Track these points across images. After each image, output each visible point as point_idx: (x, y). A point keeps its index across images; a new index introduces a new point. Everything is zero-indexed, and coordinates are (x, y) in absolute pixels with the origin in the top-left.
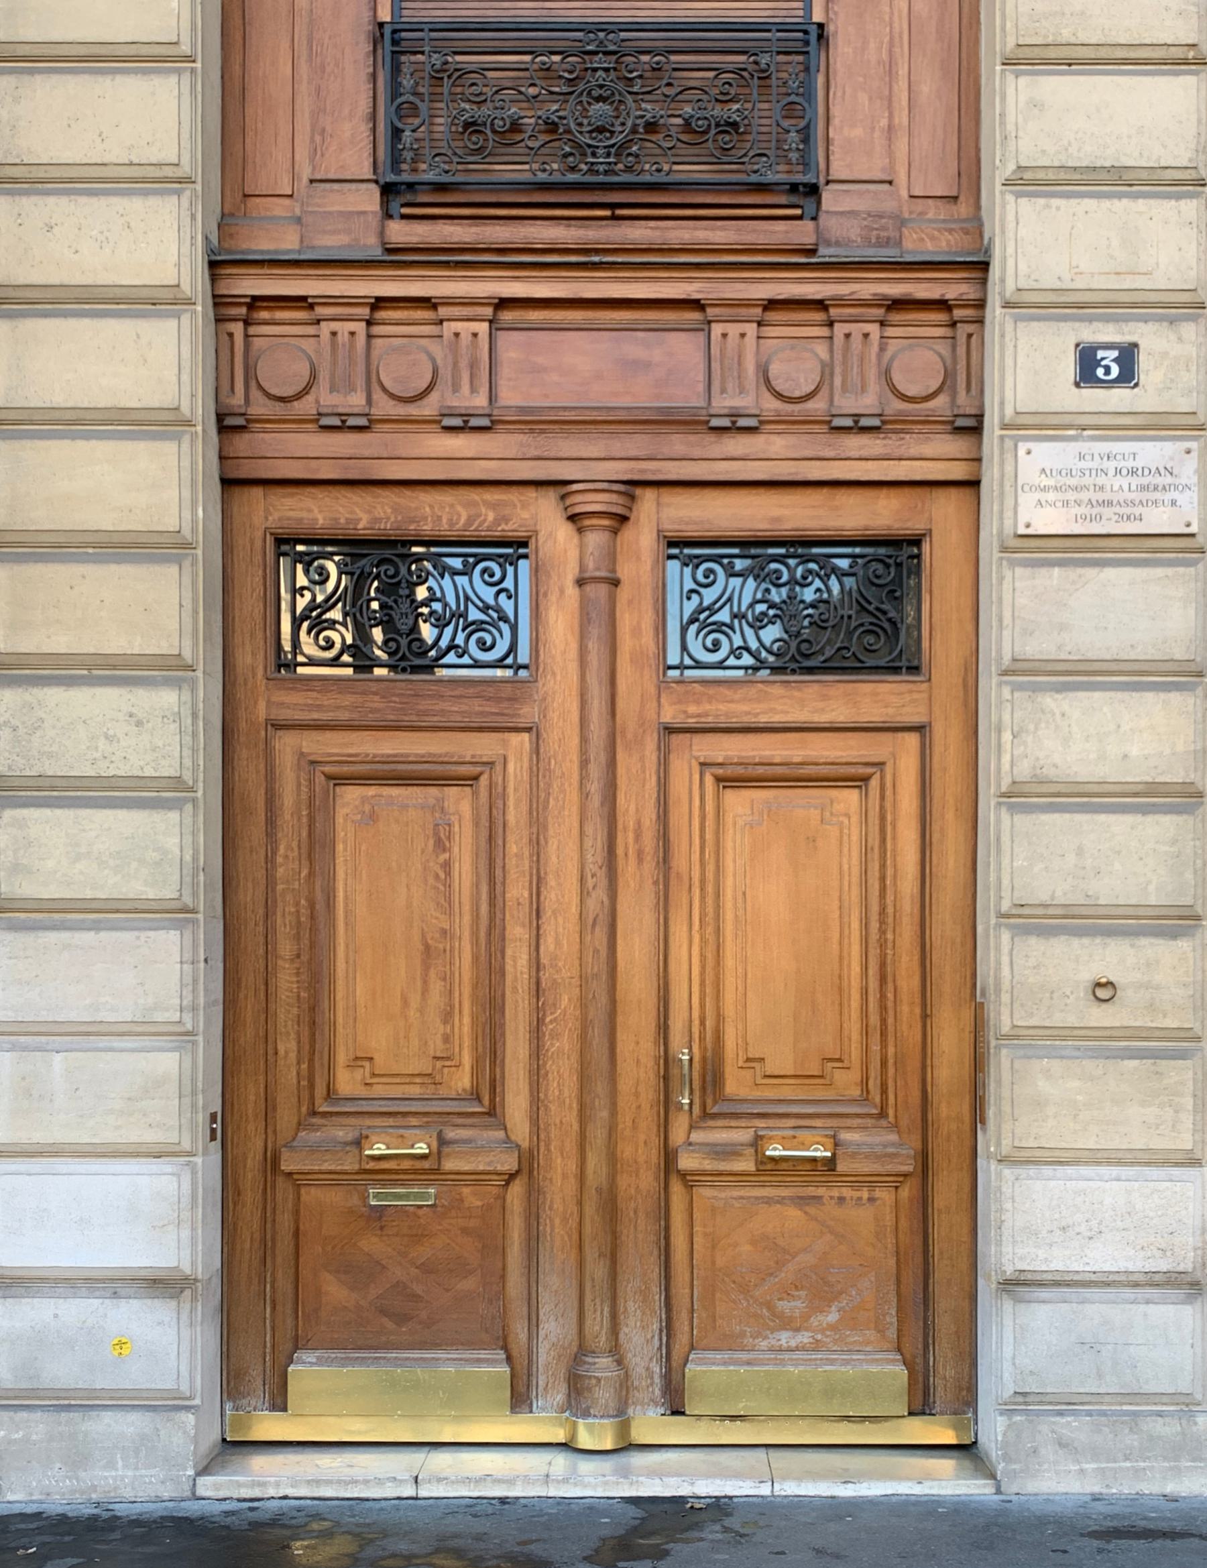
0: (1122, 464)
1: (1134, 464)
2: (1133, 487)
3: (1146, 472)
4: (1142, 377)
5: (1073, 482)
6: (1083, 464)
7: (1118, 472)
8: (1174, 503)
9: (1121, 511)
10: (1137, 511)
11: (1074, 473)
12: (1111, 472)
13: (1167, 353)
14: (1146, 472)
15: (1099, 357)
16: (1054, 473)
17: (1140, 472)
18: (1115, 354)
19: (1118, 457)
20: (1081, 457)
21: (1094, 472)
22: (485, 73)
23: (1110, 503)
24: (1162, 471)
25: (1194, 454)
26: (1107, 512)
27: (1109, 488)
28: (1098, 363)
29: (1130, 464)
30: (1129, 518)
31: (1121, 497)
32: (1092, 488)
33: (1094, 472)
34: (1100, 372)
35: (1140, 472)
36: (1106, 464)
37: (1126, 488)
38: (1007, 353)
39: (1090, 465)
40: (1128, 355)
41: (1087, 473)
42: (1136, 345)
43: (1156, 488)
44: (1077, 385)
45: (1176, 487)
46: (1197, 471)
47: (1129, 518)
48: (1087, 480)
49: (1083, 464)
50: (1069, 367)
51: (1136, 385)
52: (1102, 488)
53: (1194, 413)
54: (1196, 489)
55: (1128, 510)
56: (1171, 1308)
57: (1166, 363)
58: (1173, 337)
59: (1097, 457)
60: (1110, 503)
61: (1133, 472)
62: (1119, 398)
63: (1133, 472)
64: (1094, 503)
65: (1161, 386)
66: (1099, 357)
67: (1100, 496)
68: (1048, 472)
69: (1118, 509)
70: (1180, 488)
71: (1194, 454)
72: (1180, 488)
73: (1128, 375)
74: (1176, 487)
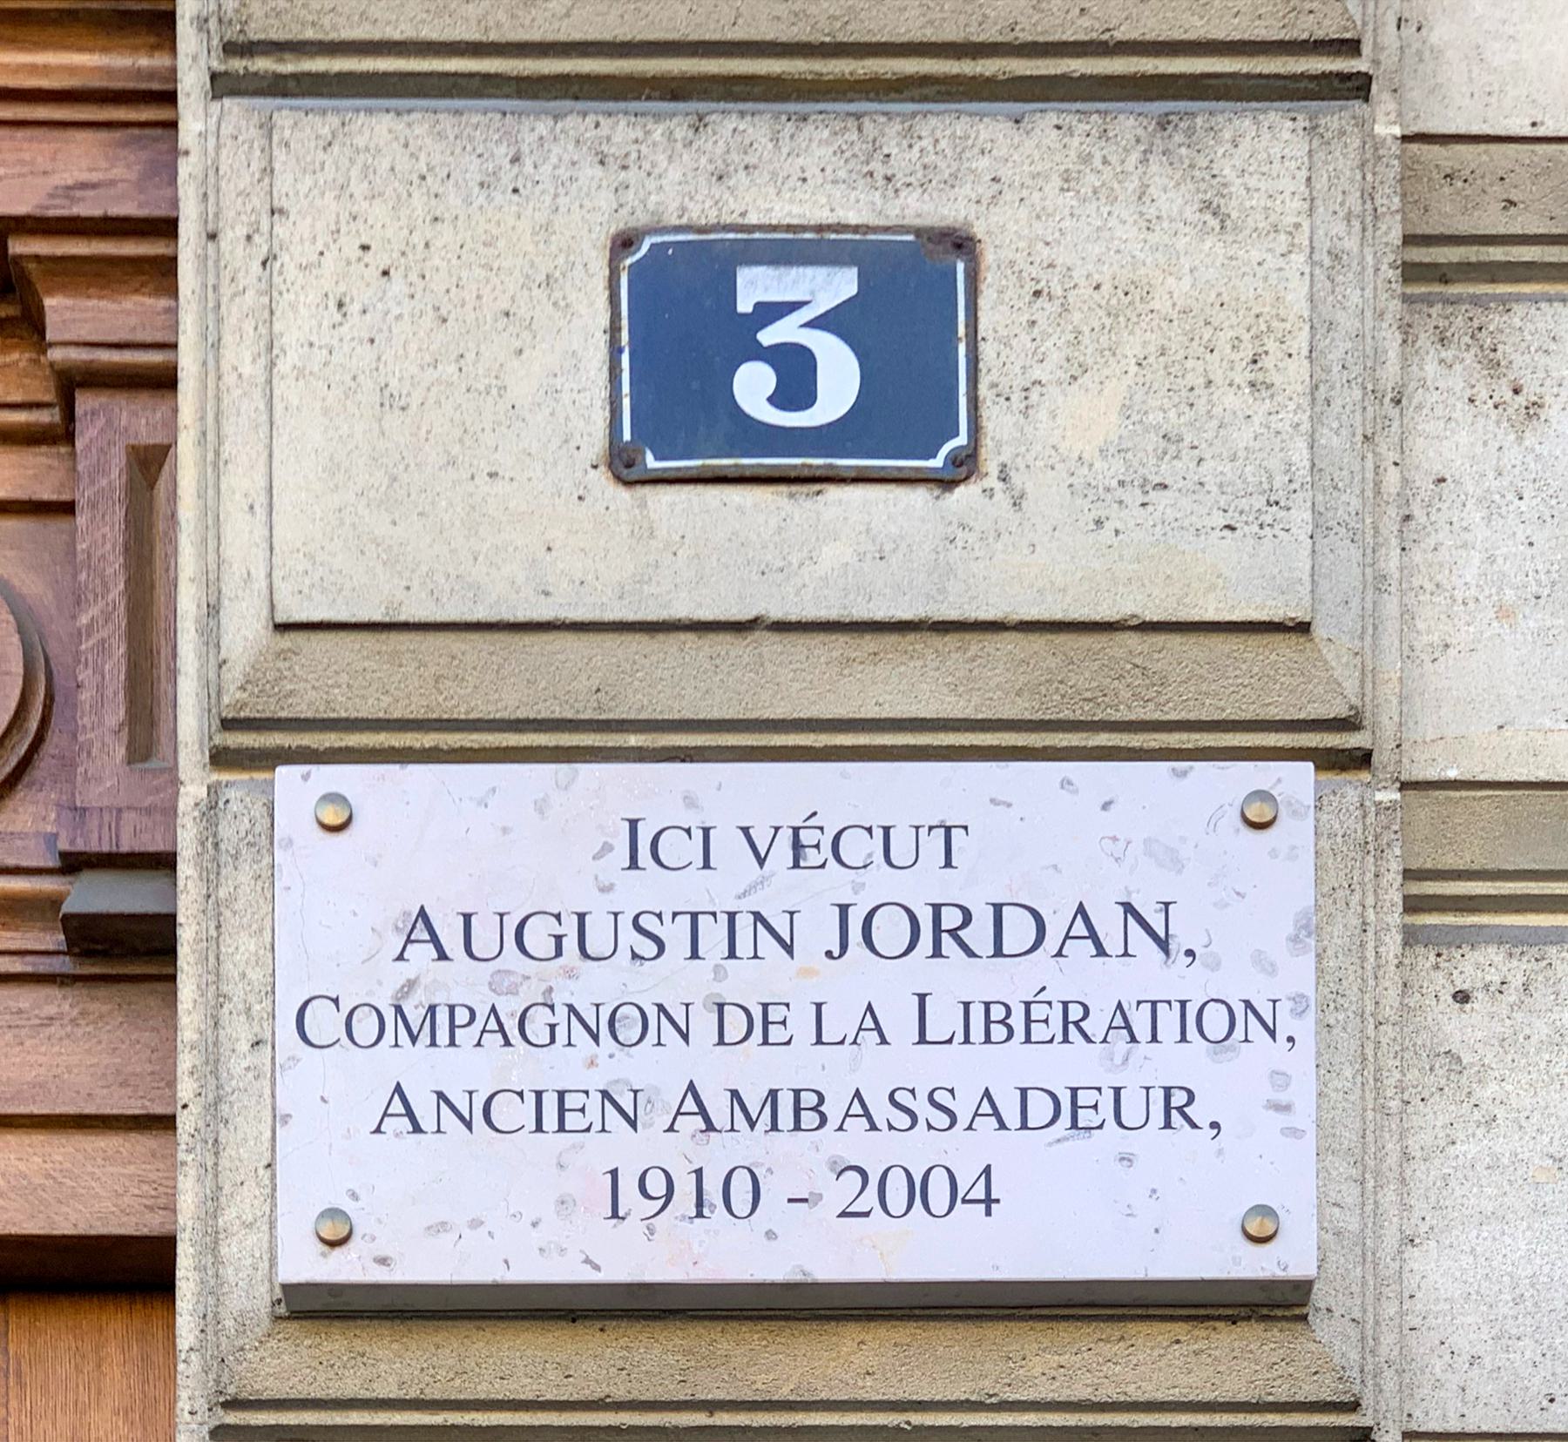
0: (880, 885)
1: (948, 887)
2: (944, 1020)
3: (1019, 931)
4: (996, 420)
5: (593, 987)
6: (647, 891)
7: (854, 930)
8: (1176, 1107)
9: (874, 1151)
10: (964, 1153)
11: (598, 941)
12: (817, 932)
13: (1134, 293)
14: (1019, 931)
15: (745, 306)
16: (484, 940)
17: (979, 935)
18: (836, 286)
19: (856, 847)
20: (641, 848)
21: (713, 936)
22: (72, 193)
23: (808, 1109)
24: (1109, 924)
25: (1295, 831)
26: (794, 1160)
27: (801, 1024)
28: (740, 337)
29: (923, 886)
30: (918, 1191)
31: (877, 1069)
32: (703, 1025)
33: (713, 936)
34: (753, 386)
35: (979, 935)
36: (782, 888)
37: (899, 1020)
38: (232, 313)
39: (693, 890)
40: (914, 297)
41: (676, 934)
42: (961, 243)
43: (1073, 1025)
44: (623, 466)
45: (1191, 1021)
46: (1311, 929)
47: (918, 1191)
48: (675, 981)
49: (647, 891)
50: (571, 365)
51: (965, 466)
52: (764, 1023)
53: (1303, 628)
54: (1305, 1029)
55: (917, 1150)
56: (179, 1320)
57: (1132, 347)
58: (1173, 198)
59: (728, 844)
60: (808, 1109)
61: (940, 931)
62: (855, 543)
63: (940, 931)
64: (719, 1109)
65: (1109, 471)
66: (745, 306)
67: (755, 1067)
68: (452, 940)
69: (856, 1144)
70: (1216, 1021)
71: (1295, 831)
72: (1216, 1021)
73: (916, 415)
74: (1191, 1021)
